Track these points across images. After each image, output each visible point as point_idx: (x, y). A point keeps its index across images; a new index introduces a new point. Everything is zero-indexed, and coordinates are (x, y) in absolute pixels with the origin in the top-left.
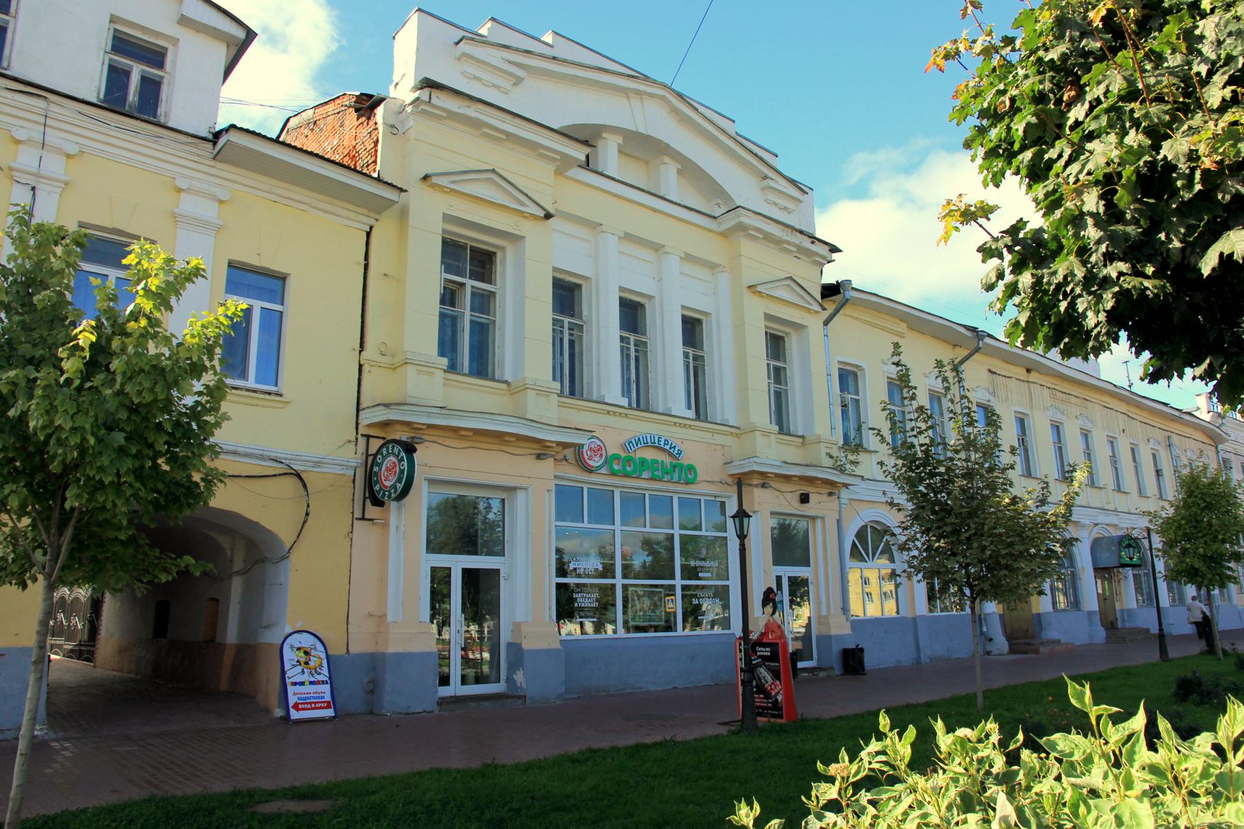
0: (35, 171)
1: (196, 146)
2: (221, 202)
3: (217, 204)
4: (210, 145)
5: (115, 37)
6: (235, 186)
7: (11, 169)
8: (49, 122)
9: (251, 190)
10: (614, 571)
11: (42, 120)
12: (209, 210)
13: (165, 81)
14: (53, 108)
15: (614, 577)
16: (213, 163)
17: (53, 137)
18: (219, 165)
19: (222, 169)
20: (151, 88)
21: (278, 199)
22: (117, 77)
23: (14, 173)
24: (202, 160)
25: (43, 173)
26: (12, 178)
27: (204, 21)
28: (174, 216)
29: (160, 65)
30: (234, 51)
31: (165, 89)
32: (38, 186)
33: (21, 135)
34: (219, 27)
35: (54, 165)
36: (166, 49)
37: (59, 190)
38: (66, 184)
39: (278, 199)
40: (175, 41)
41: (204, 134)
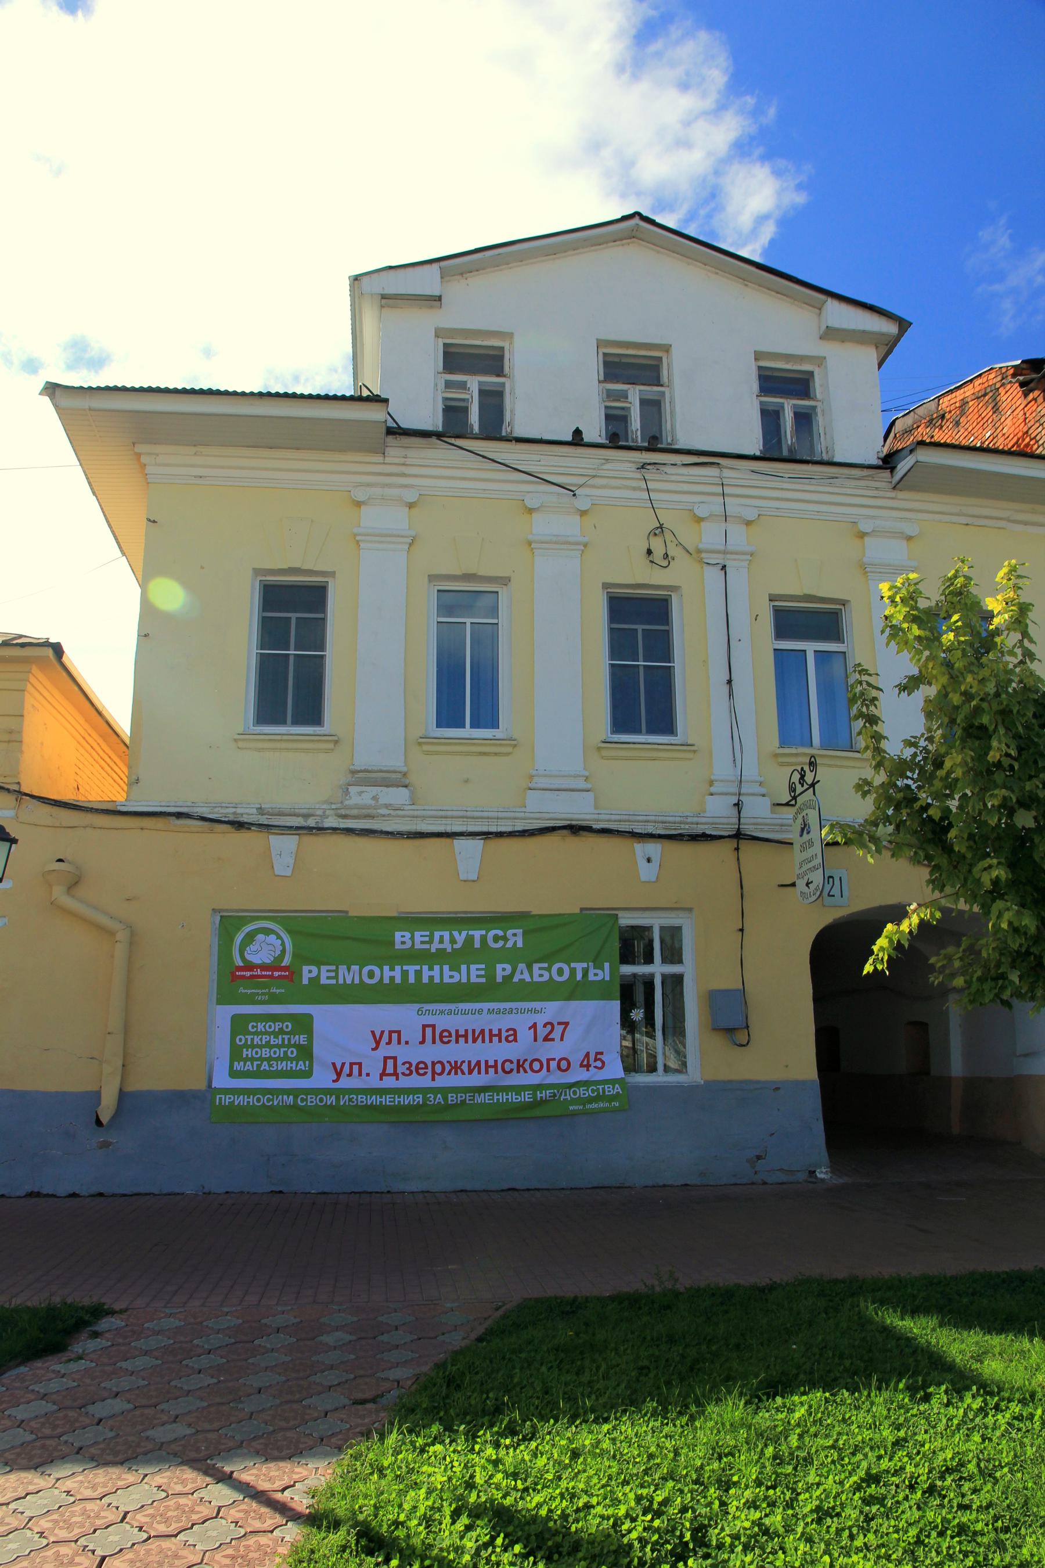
0: (722, 548)
1: (872, 478)
2: (909, 538)
3: (905, 542)
4: (886, 474)
5: (760, 377)
6: (920, 516)
7: (699, 551)
8: (727, 490)
9: (937, 517)
10: (672, 962)
11: (719, 490)
12: (396, 519)
13: (819, 410)
14: (726, 473)
15: (652, 976)
16: (893, 494)
17: (734, 506)
18: (901, 495)
19: (906, 499)
20: (493, 402)
21: (969, 520)
22: (770, 419)
23: (704, 555)
24: (882, 494)
25: (730, 548)
26: (701, 561)
27: (845, 325)
28: (530, 543)
29: (499, 372)
30: (884, 350)
31: (667, 407)
32: (728, 564)
33: (701, 512)
34: (861, 326)
35: (738, 536)
36: (502, 349)
37: (746, 564)
38: (585, 545)
39: (969, 520)
40: (820, 361)
41: (874, 461)
